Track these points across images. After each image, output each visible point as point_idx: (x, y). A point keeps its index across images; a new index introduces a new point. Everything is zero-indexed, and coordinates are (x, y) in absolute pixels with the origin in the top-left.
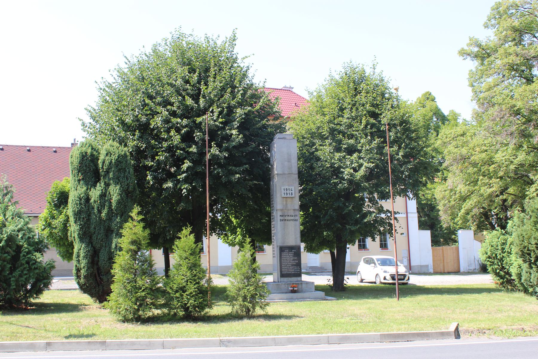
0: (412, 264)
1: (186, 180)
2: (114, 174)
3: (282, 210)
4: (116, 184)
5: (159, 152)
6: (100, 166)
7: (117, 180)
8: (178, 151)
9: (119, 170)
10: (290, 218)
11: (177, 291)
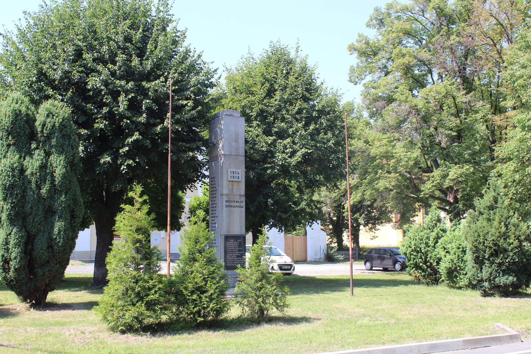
1: (128, 156)
2: (57, 140)
3: (227, 195)
4: (60, 153)
5: (98, 119)
6: (39, 129)
7: (61, 149)
8: (125, 120)
9: (63, 136)
10: (235, 204)
11: (192, 293)
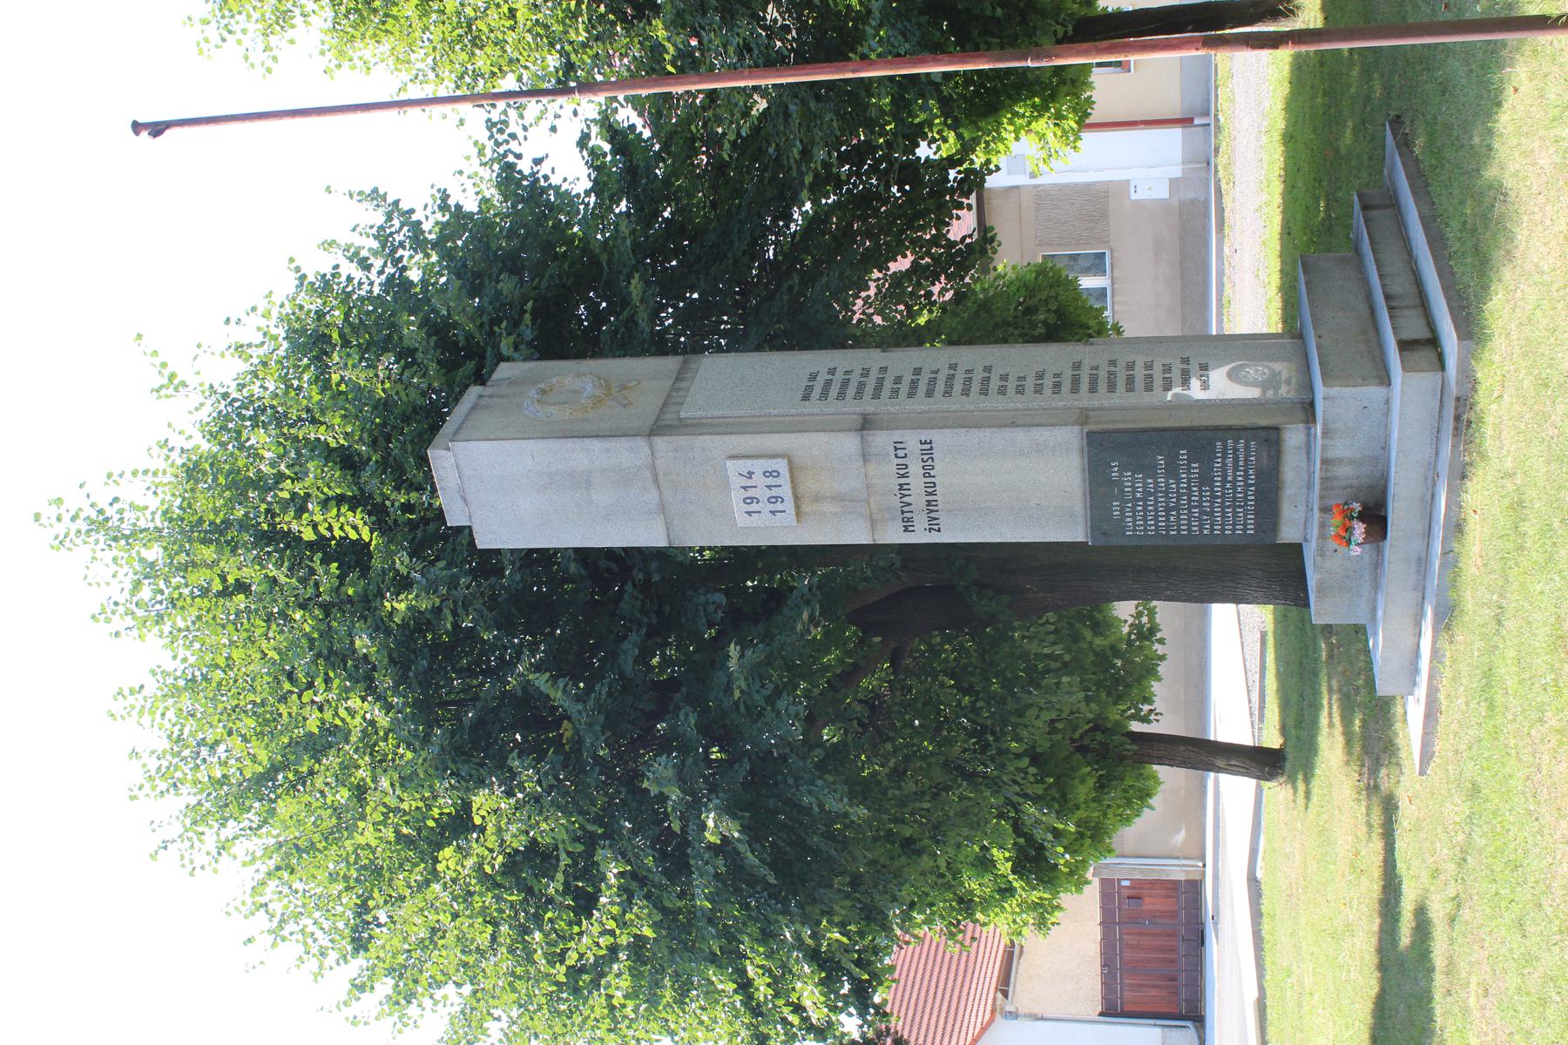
10: (916, 482)
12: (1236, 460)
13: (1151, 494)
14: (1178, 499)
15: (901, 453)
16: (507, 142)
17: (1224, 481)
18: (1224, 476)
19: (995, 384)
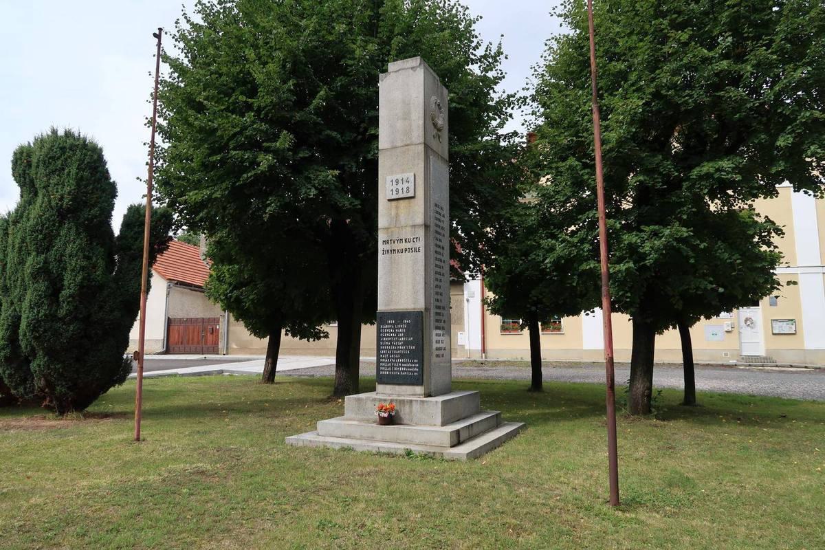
0: (696, 359)
10: (404, 246)
12: (410, 367)
13: (397, 335)
14: (395, 345)
15: (415, 240)
16: (518, 104)
17: (402, 363)
18: (404, 363)
19: (439, 277)
